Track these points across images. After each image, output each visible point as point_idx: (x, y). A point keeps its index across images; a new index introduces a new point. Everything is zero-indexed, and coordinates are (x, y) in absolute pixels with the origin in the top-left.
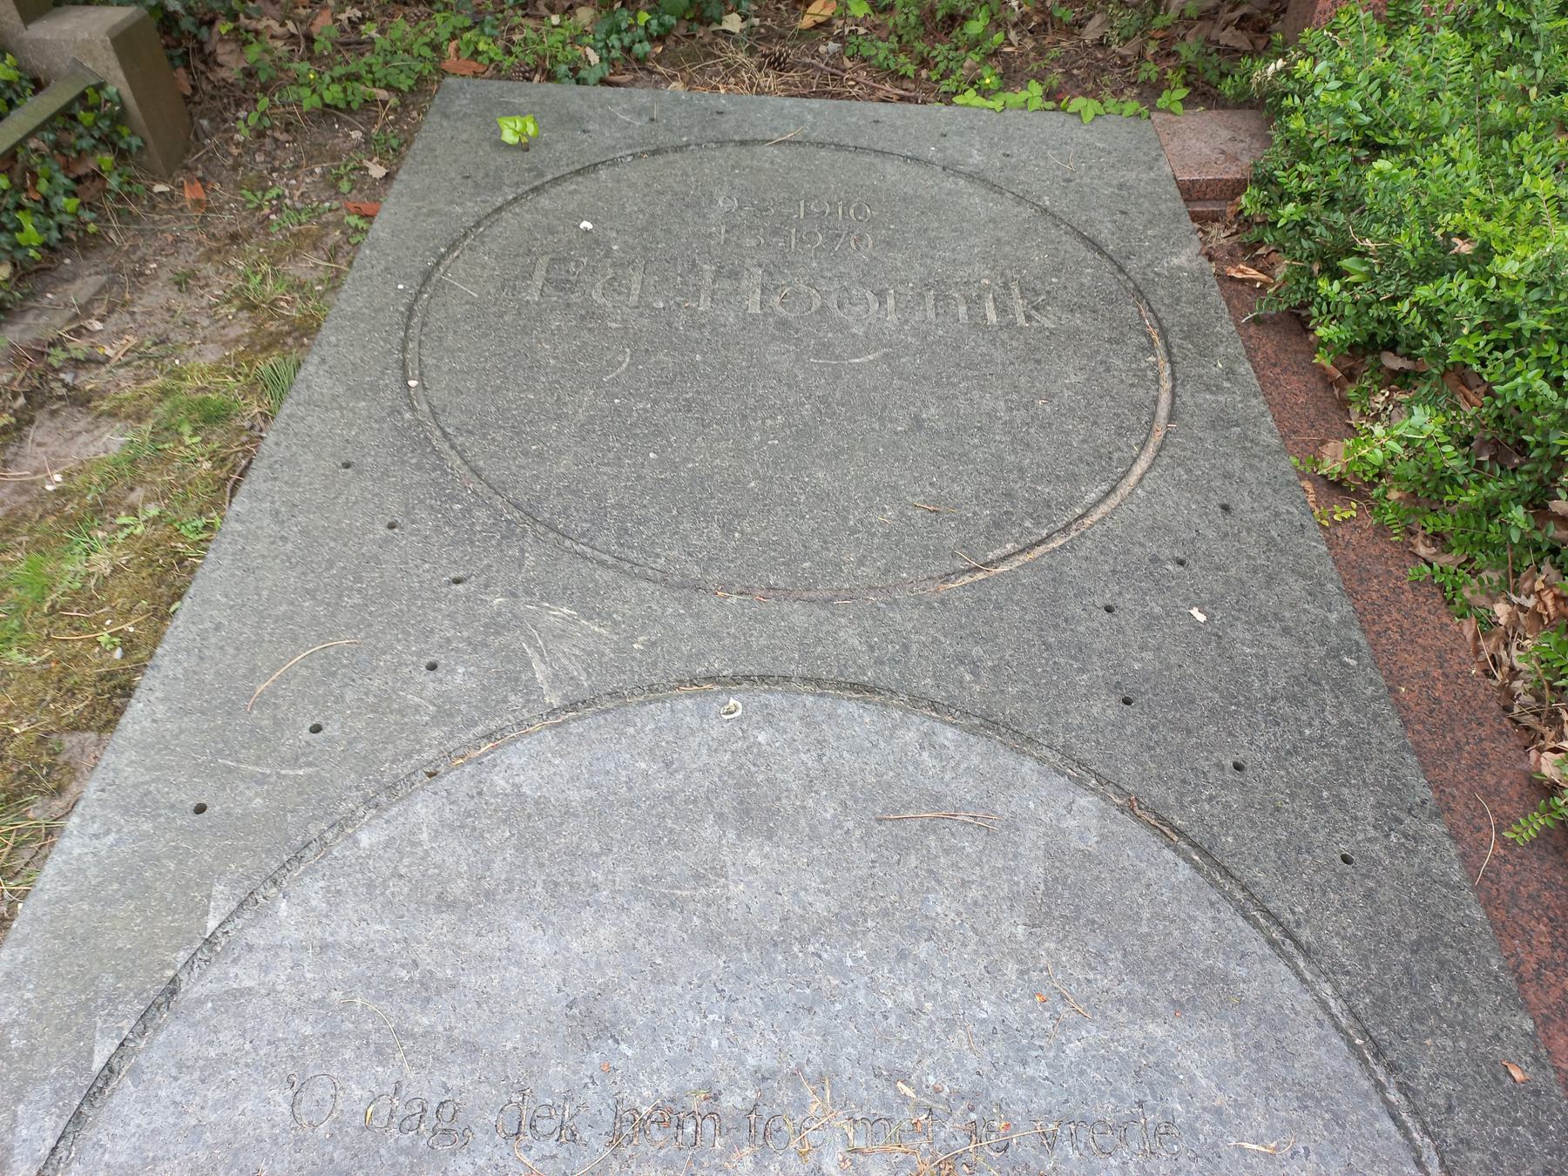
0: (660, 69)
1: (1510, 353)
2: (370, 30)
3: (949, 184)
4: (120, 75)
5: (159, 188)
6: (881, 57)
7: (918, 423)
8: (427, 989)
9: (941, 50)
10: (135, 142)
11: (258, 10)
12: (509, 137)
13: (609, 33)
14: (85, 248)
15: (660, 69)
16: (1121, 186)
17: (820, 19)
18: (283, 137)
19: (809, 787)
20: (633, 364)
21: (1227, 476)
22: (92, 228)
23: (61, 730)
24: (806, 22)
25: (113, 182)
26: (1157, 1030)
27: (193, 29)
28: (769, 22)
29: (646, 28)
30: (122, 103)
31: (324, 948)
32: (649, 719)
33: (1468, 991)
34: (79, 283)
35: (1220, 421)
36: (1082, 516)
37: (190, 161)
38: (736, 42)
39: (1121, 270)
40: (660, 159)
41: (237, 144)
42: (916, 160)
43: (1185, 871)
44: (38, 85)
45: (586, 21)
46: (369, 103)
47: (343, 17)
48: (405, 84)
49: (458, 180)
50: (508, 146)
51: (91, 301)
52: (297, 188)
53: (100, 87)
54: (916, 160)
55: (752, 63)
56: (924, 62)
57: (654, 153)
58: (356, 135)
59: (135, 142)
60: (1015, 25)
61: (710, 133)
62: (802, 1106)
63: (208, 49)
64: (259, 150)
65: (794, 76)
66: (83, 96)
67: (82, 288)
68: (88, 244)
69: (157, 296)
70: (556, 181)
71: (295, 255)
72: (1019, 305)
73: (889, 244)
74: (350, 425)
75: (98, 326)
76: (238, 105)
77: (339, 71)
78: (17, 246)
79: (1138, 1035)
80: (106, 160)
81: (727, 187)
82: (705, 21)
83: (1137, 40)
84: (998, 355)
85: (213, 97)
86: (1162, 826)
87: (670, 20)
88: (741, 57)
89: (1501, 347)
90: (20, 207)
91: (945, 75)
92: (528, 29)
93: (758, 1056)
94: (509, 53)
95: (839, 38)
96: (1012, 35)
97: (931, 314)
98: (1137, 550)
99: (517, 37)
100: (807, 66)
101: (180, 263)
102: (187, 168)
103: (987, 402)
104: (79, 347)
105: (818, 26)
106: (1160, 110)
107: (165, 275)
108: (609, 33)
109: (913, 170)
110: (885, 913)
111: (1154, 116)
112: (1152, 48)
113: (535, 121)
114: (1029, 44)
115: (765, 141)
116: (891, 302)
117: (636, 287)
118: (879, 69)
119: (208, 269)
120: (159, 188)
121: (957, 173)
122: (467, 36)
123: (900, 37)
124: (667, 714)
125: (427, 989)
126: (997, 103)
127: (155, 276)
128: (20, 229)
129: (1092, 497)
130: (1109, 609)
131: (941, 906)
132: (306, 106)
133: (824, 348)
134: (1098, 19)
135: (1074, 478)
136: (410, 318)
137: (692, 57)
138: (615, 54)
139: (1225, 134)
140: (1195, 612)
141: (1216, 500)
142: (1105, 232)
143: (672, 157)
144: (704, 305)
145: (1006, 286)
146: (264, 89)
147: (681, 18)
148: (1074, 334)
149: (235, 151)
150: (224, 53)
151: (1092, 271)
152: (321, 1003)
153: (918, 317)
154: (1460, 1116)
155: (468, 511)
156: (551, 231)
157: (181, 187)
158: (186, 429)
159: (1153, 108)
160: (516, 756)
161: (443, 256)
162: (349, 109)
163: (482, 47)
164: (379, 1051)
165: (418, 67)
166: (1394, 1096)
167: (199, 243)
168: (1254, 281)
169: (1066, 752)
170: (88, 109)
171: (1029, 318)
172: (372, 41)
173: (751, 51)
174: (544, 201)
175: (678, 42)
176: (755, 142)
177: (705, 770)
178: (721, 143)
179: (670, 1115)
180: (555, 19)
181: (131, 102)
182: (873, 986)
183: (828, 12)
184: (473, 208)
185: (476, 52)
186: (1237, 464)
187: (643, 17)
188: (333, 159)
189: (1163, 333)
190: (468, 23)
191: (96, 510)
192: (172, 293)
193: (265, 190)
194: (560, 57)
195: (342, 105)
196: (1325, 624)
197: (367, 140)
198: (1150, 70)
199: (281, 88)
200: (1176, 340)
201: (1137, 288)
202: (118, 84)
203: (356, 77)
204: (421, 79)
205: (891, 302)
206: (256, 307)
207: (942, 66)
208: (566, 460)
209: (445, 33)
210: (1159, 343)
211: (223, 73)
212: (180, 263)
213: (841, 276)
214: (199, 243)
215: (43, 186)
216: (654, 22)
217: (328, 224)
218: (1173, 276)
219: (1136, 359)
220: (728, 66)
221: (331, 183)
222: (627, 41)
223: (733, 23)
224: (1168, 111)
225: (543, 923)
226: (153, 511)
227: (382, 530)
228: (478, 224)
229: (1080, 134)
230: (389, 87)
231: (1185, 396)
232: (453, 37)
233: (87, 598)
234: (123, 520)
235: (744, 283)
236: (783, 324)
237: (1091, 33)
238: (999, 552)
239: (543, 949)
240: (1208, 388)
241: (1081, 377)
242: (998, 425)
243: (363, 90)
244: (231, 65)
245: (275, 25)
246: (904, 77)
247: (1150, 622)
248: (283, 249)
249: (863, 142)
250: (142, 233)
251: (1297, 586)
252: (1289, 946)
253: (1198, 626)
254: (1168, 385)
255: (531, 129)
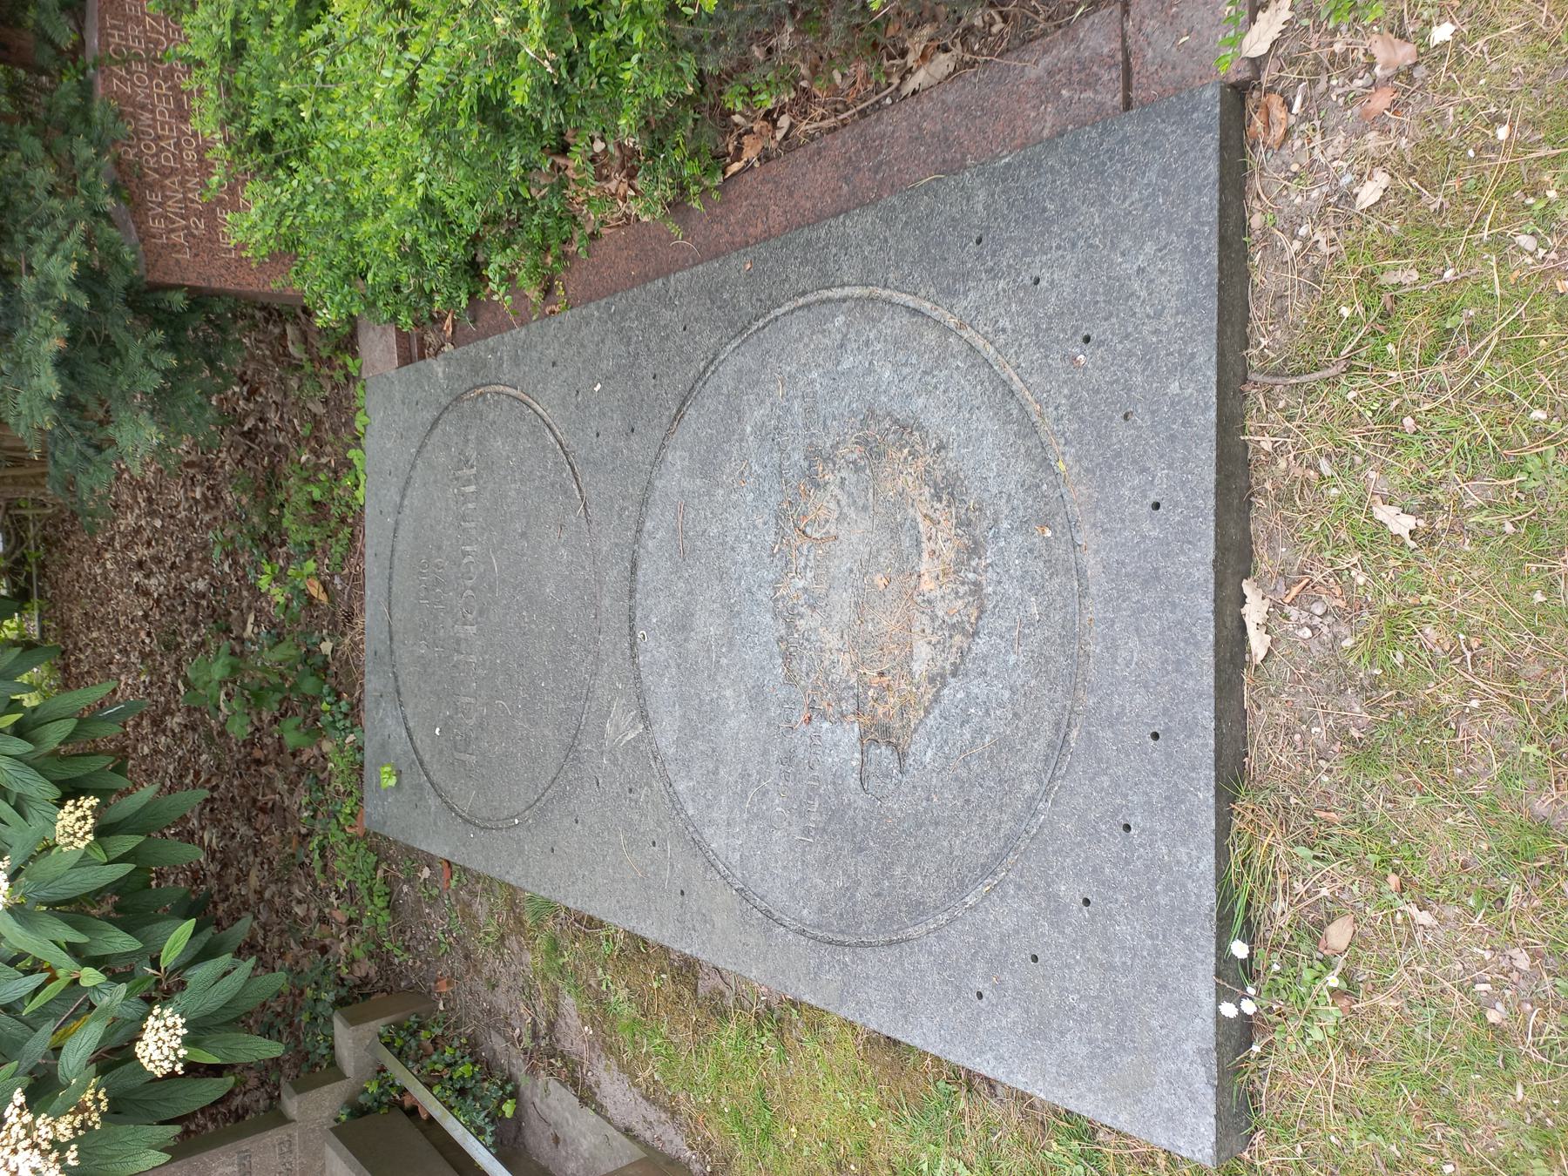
0: (357, 694)
1: (454, 227)
2: (343, 885)
3: (407, 511)
4: (373, 1023)
5: (441, 1007)
6: (341, 549)
7: (523, 535)
8: (745, 775)
9: (334, 510)
10: (413, 1018)
11: (334, 956)
12: (393, 782)
13: (337, 729)
14: (476, 1045)
15: (357, 694)
16: (404, 403)
17: (321, 589)
18: (408, 934)
19: (673, 595)
20: (503, 698)
21: (540, 360)
22: (464, 1041)
23: (696, 998)
24: (323, 598)
25: (438, 1031)
26: (749, 429)
27: (346, 989)
28: (325, 623)
29: (331, 704)
30: (390, 1025)
31: (729, 824)
32: (649, 680)
33: (725, 281)
34: (496, 1047)
35: (516, 361)
36: (561, 445)
37: (426, 991)
38: (338, 645)
39: (447, 408)
40: (402, 690)
41: (415, 962)
42: (395, 530)
43: (691, 411)
44: (383, 1070)
45: (330, 745)
46: (386, 882)
47: (335, 903)
48: (373, 858)
49: (418, 811)
50: (398, 783)
51: (505, 1037)
52: (438, 924)
53: (380, 1036)
54: (395, 530)
55: (350, 634)
56: (343, 520)
57: (399, 694)
58: (405, 888)
59: (413, 1018)
60: (318, 458)
61: (387, 658)
62: (783, 597)
63: (358, 982)
64: (416, 949)
65: (356, 605)
66: (387, 1045)
67: (498, 1043)
68: (472, 1048)
69: (501, 1000)
70: (416, 752)
71: (475, 917)
72: (466, 471)
73: (439, 548)
74: (535, 852)
75: (518, 1031)
76: (392, 964)
77: (366, 901)
78: (472, 1077)
79: (752, 438)
80: (424, 1034)
81: (415, 648)
82: (326, 666)
83: (321, 380)
84: (490, 486)
85: (387, 979)
86: (678, 417)
87: (326, 689)
88: (347, 641)
89: (452, 231)
90: (451, 1078)
91: (350, 507)
92: (337, 783)
93: (768, 618)
94: (351, 793)
95: (332, 576)
96: (324, 460)
97: (473, 524)
98: (574, 416)
99: (342, 790)
100: (350, 597)
101: (482, 988)
102: (429, 992)
103: (512, 494)
104: (527, 1041)
105: (325, 590)
106: (360, 373)
107: (490, 997)
108: (337, 729)
109: (401, 533)
110: (719, 558)
111: (364, 376)
112: (325, 371)
113: (383, 766)
114: (328, 449)
115: (390, 626)
116: (468, 548)
117: (467, 699)
118: (348, 550)
119: (485, 971)
120: (441, 1007)
121: (401, 505)
122: (341, 820)
123: (329, 537)
124: (645, 669)
125: (745, 775)
126: (362, 477)
127: (491, 1003)
128: (462, 1077)
129: (552, 439)
130: (598, 435)
131: (714, 531)
132: (389, 919)
133: (491, 589)
134: (310, 405)
135: (544, 447)
136: (487, 828)
137: (349, 674)
138: (348, 724)
139: (371, 334)
140: (596, 389)
141: (550, 369)
142: (428, 415)
143: (400, 683)
144: (473, 659)
145: (457, 479)
146: (380, 946)
147: (325, 682)
148: (480, 441)
149: (418, 963)
150: (360, 972)
151: (447, 427)
152: (747, 822)
153: (474, 532)
154: (763, 296)
155: (569, 782)
156: (441, 752)
157: (440, 994)
158: (561, 961)
159: (359, 378)
160: (663, 743)
161: (457, 814)
162: (390, 894)
163: (348, 811)
164: (764, 794)
165: (362, 851)
166: (761, 323)
167: (472, 979)
168: (453, 320)
169: (653, 465)
170: (393, 1041)
171: (472, 467)
172: (349, 882)
173: (343, 634)
174: (426, 758)
175: (340, 683)
176: (390, 632)
177: (667, 648)
178: (392, 652)
179: (787, 657)
180: (331, 765)
181: (390, 1019)
182: (744, 564)
183: (316, 583)
184: (433, 802)
185: (352, 814)
186: (535, 355)
187: (325, 706)
188: (420, 901)
189: (478, 387)
190: (334, 821)
191: (599, 1002)
192: (499, 991)
193: (440, 942)
194: (351, 759)
195: (388, 898)
196: (599, 319)
197: (408, 881)
198: (339, 375)
199: (379, 937)
200: (479, 381)
201: (456, 399)
202: (378, 1025)
203: (370, 889)
204: (370, 849)
205: (468, 548)
206: (502, 935)
207: (344, 509)
208: (546, 732)
209: (341, 835)
210: (481, 390)
211: (372, 973)
212: (482, 988)
213: (457, 578)
214: (472, 979)
215: (439, 1067)
216: (328, 699)
217: (457, 899)
218: (448, 377)
219: (489, 406)
220: (353, 650)
221: (434, 901)
222: (340, 716)
223: (326, 647)
224: (360, 369)
225: (724, 722)
226: (600, 971)
227: (579, 827)
228: (440, 796)
229: (376, 424)
230: (376, 869)
231: (505, 378)
232: (344, 830)
233: (636, 996)
234: (604, 988)
235: (462, 636)
236: (481, 613)
237: (319, 409)
238: (577, 492)
239: (732, 723)
240: (501, 365)
241: (499, 438)
242: (523, 488)
243: (378, 886)
244: (366, 968)
245: (342, 945)
246: (352, 534)
247: (603, 414)
248: (471, 925)
249: (387, 564)
250: (467, 1015)
251: (585, 331)
252: (716, 362)
253: (603, 388)
254: (501, 388)
255: (387, 769)
